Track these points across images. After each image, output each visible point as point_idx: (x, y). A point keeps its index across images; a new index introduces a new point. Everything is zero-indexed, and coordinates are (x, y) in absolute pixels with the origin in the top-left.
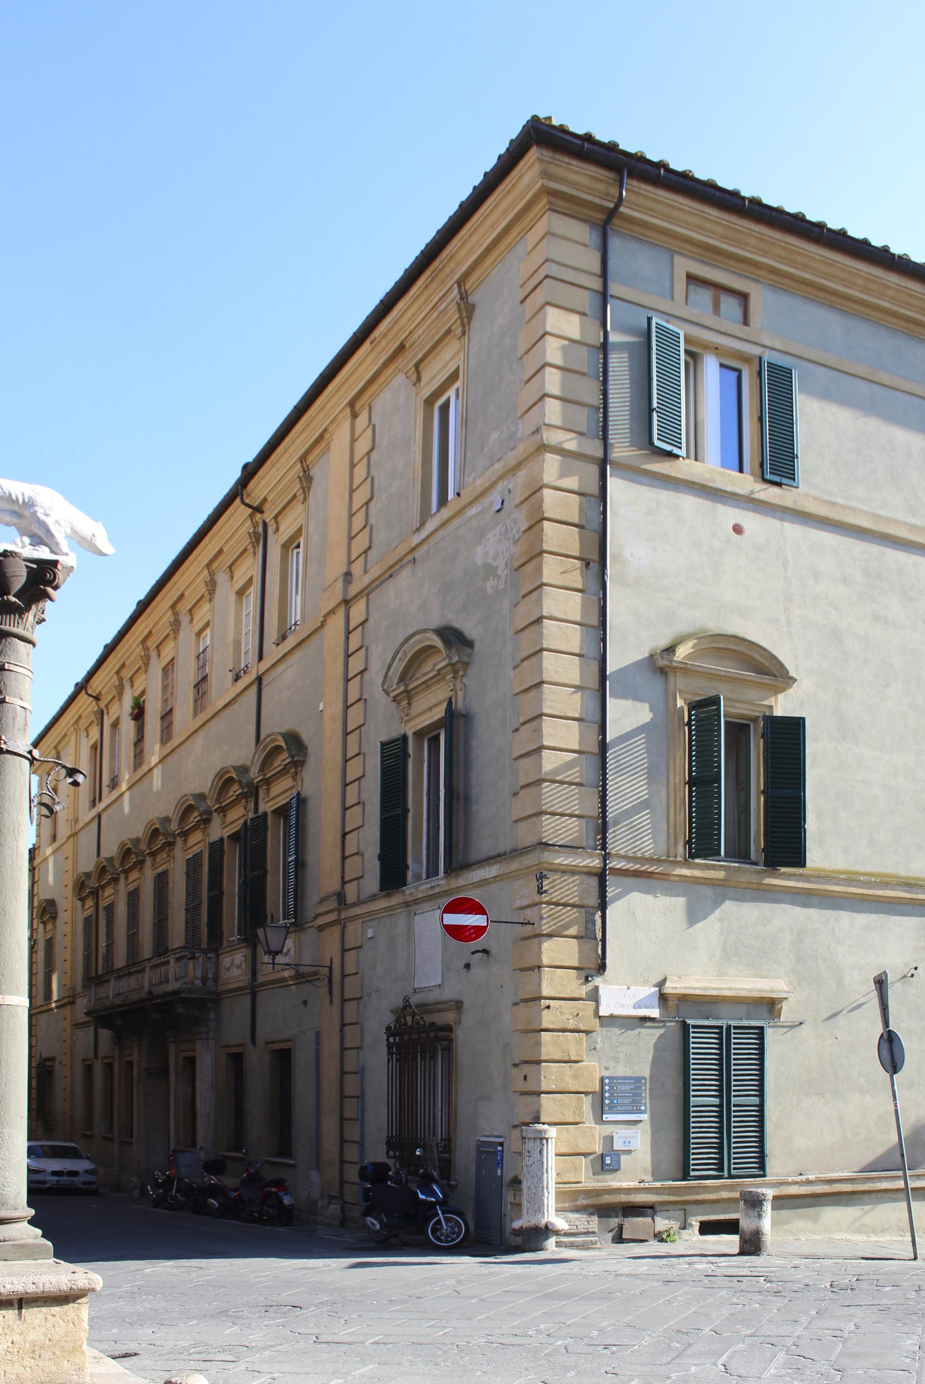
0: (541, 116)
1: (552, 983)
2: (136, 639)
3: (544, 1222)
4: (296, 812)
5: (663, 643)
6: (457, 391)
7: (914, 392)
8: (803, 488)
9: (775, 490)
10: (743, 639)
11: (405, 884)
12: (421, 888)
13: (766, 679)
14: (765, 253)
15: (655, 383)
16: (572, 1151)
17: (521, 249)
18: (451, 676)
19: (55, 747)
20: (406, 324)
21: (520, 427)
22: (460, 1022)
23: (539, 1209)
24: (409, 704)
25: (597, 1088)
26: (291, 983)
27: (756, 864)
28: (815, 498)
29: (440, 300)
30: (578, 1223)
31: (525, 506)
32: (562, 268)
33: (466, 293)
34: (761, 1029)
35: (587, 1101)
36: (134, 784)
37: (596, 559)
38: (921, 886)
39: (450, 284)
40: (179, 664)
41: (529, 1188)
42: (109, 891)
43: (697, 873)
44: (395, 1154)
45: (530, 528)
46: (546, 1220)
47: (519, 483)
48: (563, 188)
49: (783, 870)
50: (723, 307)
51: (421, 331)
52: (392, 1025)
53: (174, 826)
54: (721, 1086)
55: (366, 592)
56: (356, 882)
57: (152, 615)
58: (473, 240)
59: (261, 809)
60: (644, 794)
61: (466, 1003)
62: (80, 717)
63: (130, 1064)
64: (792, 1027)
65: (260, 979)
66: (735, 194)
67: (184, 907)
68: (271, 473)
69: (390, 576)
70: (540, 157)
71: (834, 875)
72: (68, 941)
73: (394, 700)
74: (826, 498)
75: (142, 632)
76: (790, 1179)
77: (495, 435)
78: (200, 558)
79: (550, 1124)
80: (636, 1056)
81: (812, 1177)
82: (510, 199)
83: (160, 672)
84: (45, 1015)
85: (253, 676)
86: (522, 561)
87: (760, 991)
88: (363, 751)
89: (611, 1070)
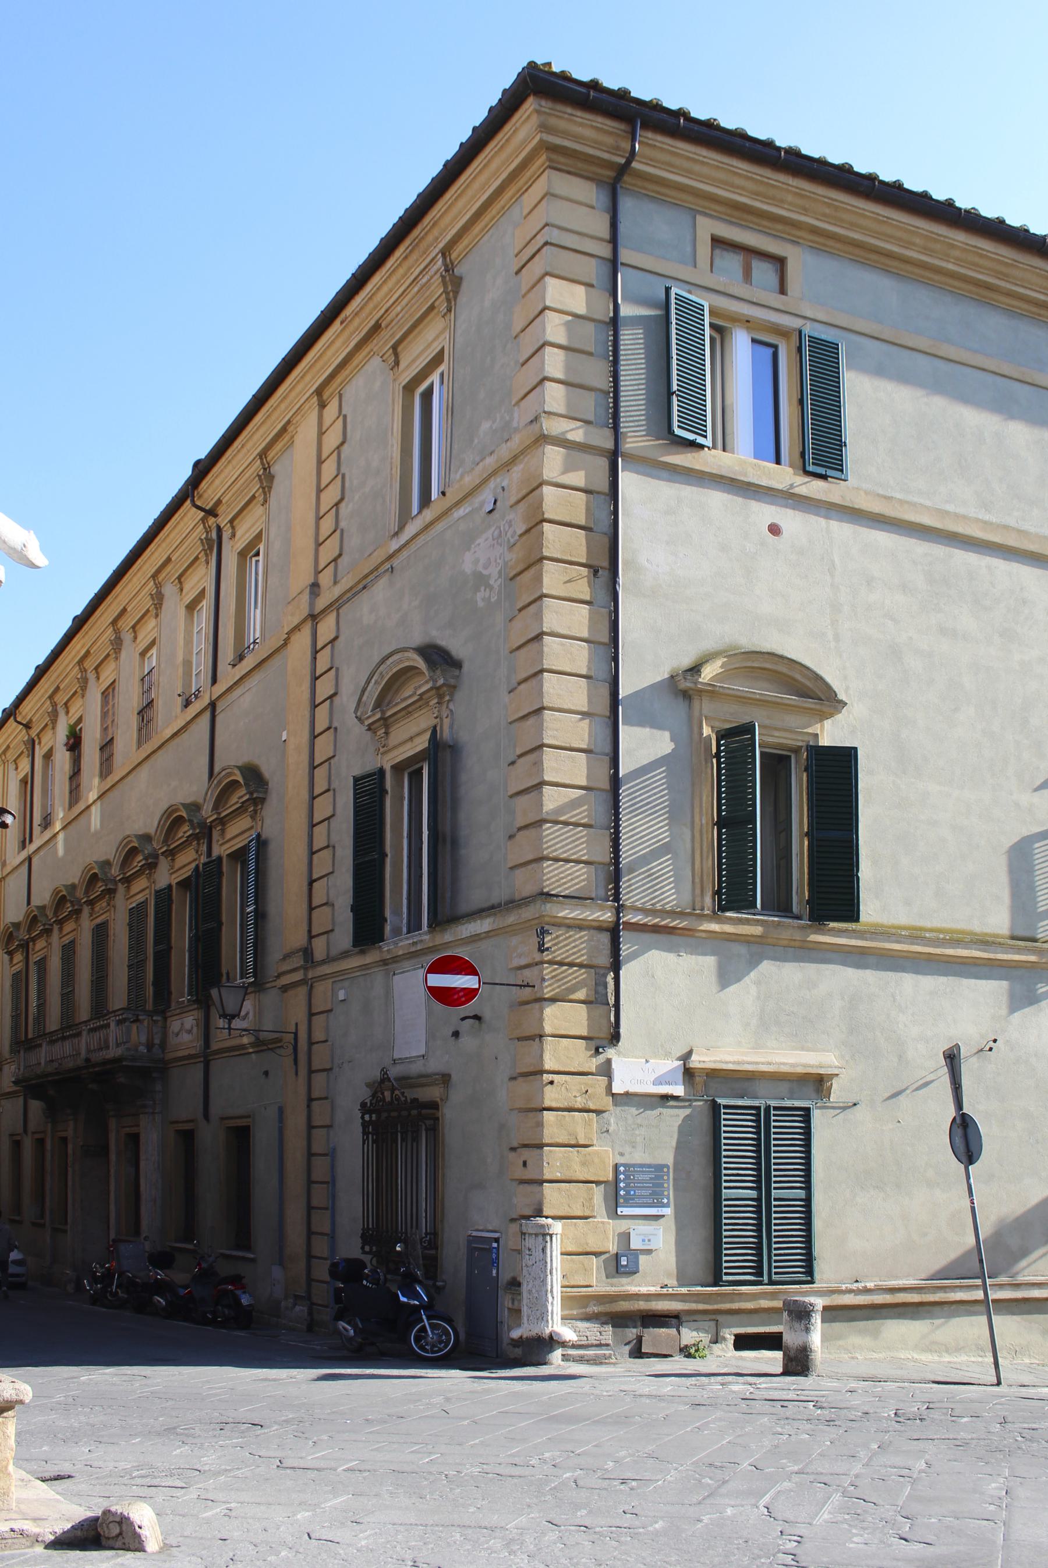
1: (554, 1055)
3: (547, 1331)
4: (255, 856)
5: (686, 662)
6: (442, 375)
7: (986, 367)
9: (819, 484)
10: (782, 657)
13: (809, 703)
14: (805, 211)
15: (674, 362)
16: (580, 1250)
17: (516, 213)
18: (436, 701)
22: (447, 1098)
23: (542, 1316)
24: (387, 733)
25: (610, 1177)
26: (251, 1050)
28: (866, 493)
29: (421, 272)
30: (588, 1334)
33: (452, 264)
34: (807, 1110)
35: (598, 1192)
37: (606, 566)
39: (433, 254)
41: (530, 1292)
42: (41, 944)
43: (728, 928)
44: (371, 1249)
46: (550, 1329)
47: (514, 480)
49: (832, 925)
50: (755, 273)
51: (399, 308)
52: (368, 1101)
53: (115, 871)
55: (336, 605)
57: (90, 633)
58: (460, 204)
60: (665, 836)
62: (8, 747)
63: (64, 1140)
64: (844, 1108)
66: (769, 144)
69: (364, 588)
70: (538, 107)
71: (894, 931)
73: (369, 729)
74: (881, 492)
75: (79, 652)
76: (844, 1287)
77: (486, 426)
78: (144, 568)
79: (554, 1218)
81: (870, 1285)
82: (504, 155)
83: (99, 695)
85: (206, 701)
87: (805, 1066)
89: (627, 1156)
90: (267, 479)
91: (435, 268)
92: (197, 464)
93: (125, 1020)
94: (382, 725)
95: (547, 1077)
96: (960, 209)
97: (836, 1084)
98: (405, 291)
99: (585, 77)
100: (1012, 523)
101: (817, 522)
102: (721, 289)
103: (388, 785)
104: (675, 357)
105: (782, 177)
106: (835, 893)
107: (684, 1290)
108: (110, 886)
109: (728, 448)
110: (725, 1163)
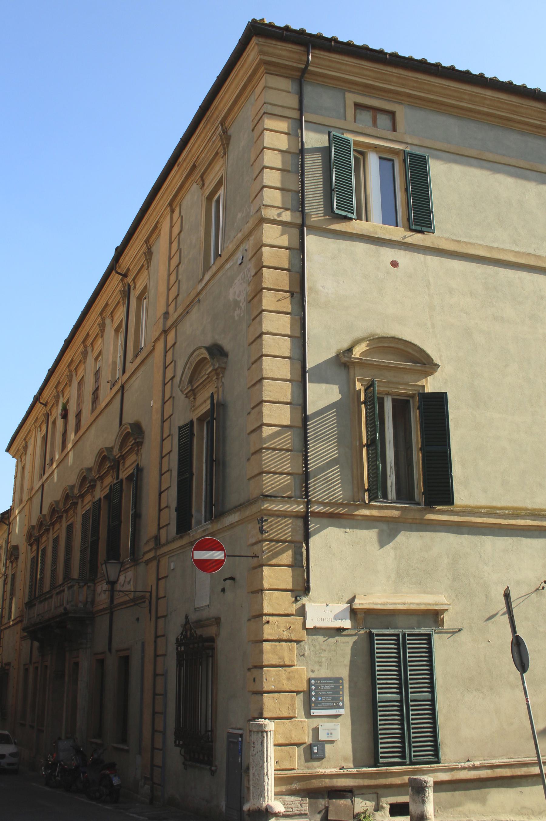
0: (258, 19)
1: (271, 603)
2: (65, 364)
3: (264, 805)
5: (345, 345)
7: (510, 164)
8: (437, 233)
9: (419, 235)
10: (400, 339)
11: (190, 528)
12: (199, 531)
13: (418, 367)
14: (404, 86)
15: (334, 172)
16: (287, 742)
17: (253, 98)
18: (215, 378)
19: (25, 439)
20: (195, 152)
21: (252, 208)
22: (219, 634)
23: (261, 793)
24: (195, 399)
25: (306, 688)
27: (418, 504)
28: (446, 239)
29: (212, 135)
30: (293, 806)
31: (254, 259)
32: (275, 107)
33: (226, 129)
34: (429, 635)
35: (299, 700)
36: (60, 462)
37: (298, 292)
38: (544, 515)
39: (217, 125)
40: (86, 379)
41: (254, 774)
43: (375, 513)
44: (179, 743)
45: (256, 274)
46: (266, 803)
47: (249, 245)
48: (274, 60)
49: (438, 508)
50: (379, 121)
51: (203, 155)
52: (179, 637)
53: (76, 491)
54: (400, 684)
55: (175, 324)
56: (166, 528)
57: (73, 348)
58: (227, 96)
59: (120, 477)
60: (335, 454)
61: (223, 620)
64: (454, 633)
65: (115, 602)
66: (381, 52)
67: (80, 549)
68: (131, 252)
69: (187, 313)
70: (258, 42)
71: (476, 510)
73: (186, 397)
74: (455, 238)
75: (68, 360)
76: (459, 765)
77: (239, 215)
78: (96, 310)
79: (270, 719)
80: (336, 661)
81: (477, 763)
82: (244, 69)
86: (252, 297)
87: (425, 604)
89: (316, 672)
91: (218, 132)
92: (117, 249)
94: (192, 394)
95: (265, 618)
96: (487, 78)
97: (447, 617)
98: (205, 145)
99: (282, 25)
100: (532, 252)
101: (419, 257)
102: (360, 131)
104: (334, 170)
105: (389, 69)
106: (439, 489)
107: (354, 771)
109: (369, 219)
110: (378, 675)
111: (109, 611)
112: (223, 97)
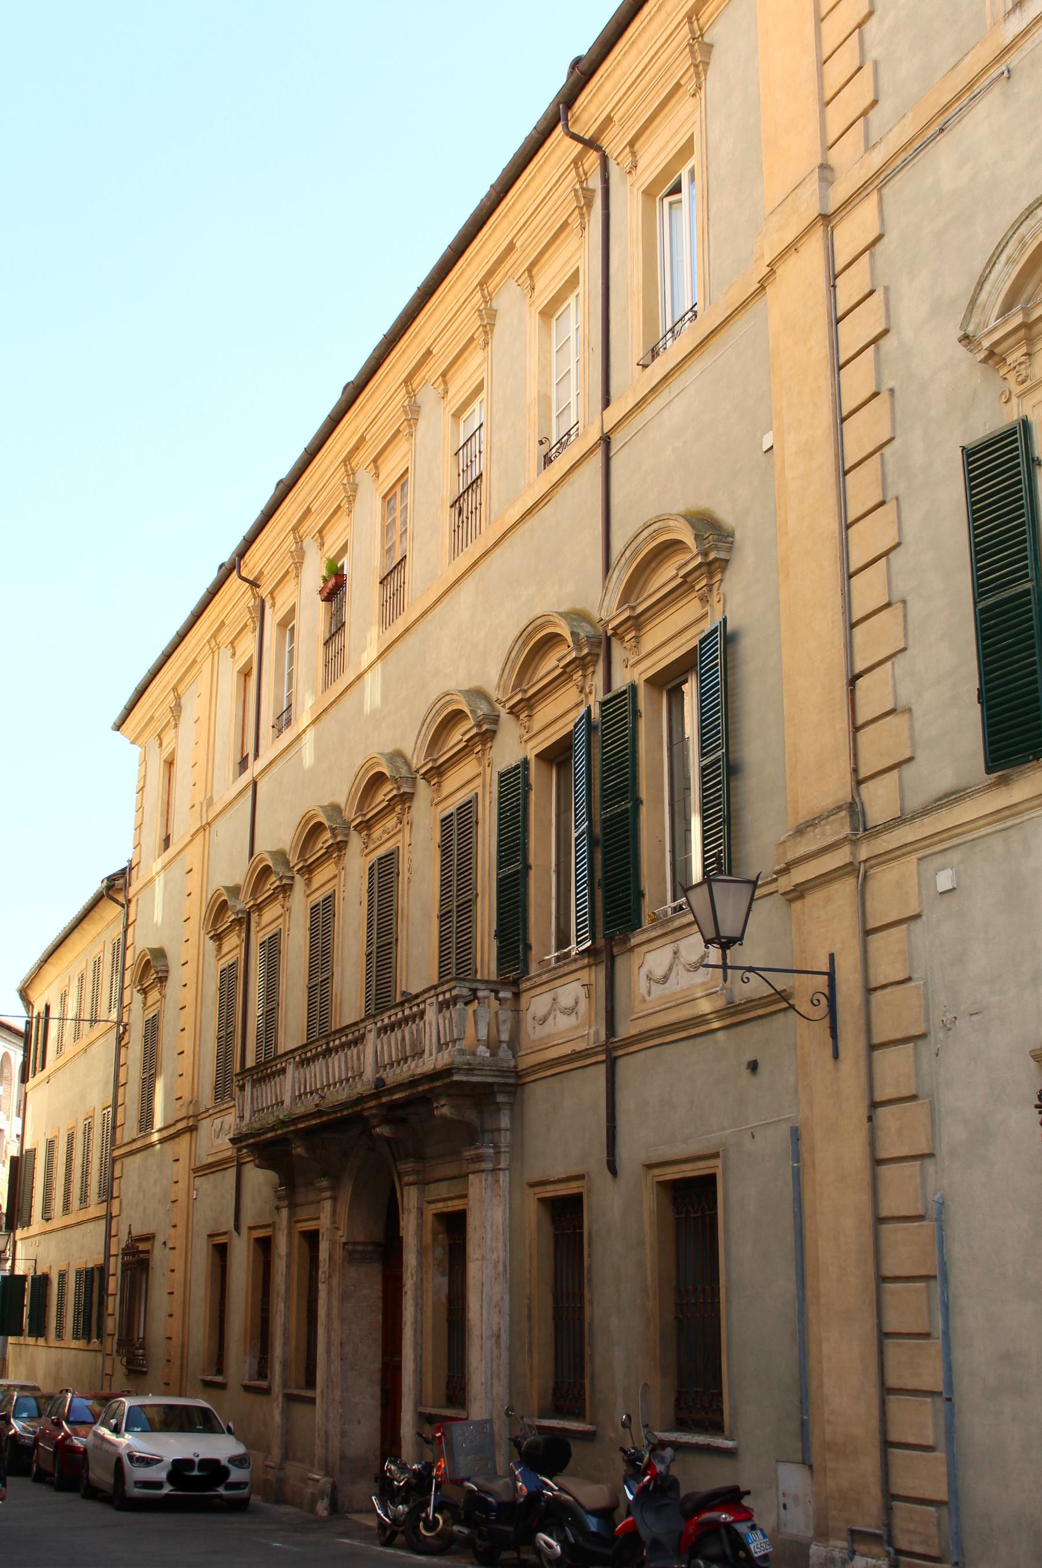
4: (714, 660)
6: (692, 172)
19: (174, 689)
55: (878, 181)
57: (368, 406)
62: (223, 624)
63: (312, 1238)
67: (435, 911)
69: (942, 130)
72: (187, 1019)
83: (379, 502)
84: (138, 1157)
85: (595, 435)
88: (890, 495)
90: (177, 709)
93: (455, 1000)
103: (642, 705)
108: (405, 789)
111: (602, 1057)
112: (613, 70)
